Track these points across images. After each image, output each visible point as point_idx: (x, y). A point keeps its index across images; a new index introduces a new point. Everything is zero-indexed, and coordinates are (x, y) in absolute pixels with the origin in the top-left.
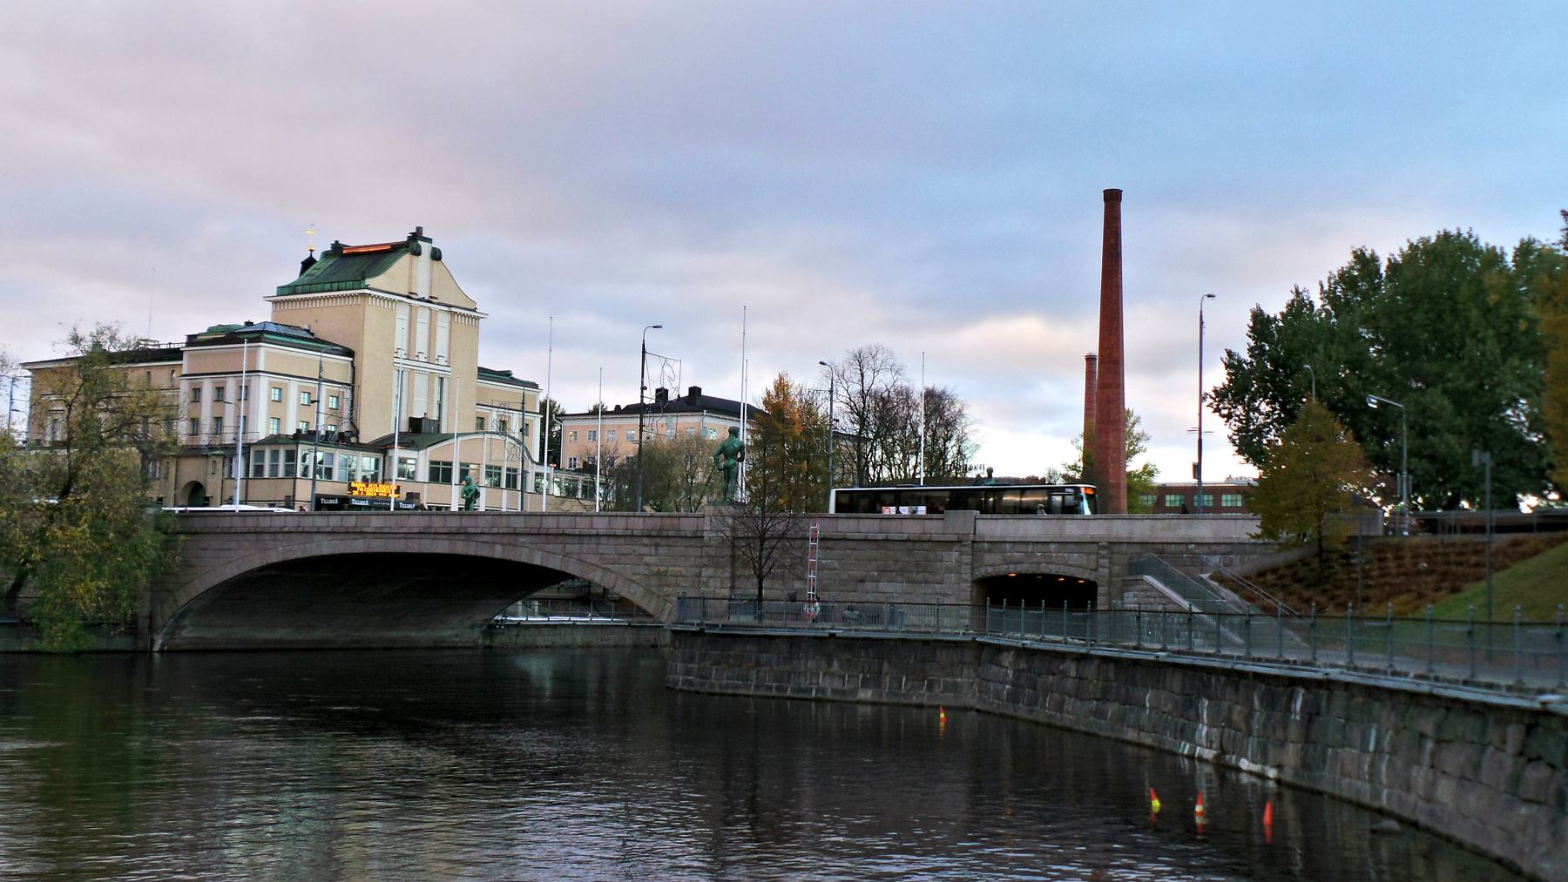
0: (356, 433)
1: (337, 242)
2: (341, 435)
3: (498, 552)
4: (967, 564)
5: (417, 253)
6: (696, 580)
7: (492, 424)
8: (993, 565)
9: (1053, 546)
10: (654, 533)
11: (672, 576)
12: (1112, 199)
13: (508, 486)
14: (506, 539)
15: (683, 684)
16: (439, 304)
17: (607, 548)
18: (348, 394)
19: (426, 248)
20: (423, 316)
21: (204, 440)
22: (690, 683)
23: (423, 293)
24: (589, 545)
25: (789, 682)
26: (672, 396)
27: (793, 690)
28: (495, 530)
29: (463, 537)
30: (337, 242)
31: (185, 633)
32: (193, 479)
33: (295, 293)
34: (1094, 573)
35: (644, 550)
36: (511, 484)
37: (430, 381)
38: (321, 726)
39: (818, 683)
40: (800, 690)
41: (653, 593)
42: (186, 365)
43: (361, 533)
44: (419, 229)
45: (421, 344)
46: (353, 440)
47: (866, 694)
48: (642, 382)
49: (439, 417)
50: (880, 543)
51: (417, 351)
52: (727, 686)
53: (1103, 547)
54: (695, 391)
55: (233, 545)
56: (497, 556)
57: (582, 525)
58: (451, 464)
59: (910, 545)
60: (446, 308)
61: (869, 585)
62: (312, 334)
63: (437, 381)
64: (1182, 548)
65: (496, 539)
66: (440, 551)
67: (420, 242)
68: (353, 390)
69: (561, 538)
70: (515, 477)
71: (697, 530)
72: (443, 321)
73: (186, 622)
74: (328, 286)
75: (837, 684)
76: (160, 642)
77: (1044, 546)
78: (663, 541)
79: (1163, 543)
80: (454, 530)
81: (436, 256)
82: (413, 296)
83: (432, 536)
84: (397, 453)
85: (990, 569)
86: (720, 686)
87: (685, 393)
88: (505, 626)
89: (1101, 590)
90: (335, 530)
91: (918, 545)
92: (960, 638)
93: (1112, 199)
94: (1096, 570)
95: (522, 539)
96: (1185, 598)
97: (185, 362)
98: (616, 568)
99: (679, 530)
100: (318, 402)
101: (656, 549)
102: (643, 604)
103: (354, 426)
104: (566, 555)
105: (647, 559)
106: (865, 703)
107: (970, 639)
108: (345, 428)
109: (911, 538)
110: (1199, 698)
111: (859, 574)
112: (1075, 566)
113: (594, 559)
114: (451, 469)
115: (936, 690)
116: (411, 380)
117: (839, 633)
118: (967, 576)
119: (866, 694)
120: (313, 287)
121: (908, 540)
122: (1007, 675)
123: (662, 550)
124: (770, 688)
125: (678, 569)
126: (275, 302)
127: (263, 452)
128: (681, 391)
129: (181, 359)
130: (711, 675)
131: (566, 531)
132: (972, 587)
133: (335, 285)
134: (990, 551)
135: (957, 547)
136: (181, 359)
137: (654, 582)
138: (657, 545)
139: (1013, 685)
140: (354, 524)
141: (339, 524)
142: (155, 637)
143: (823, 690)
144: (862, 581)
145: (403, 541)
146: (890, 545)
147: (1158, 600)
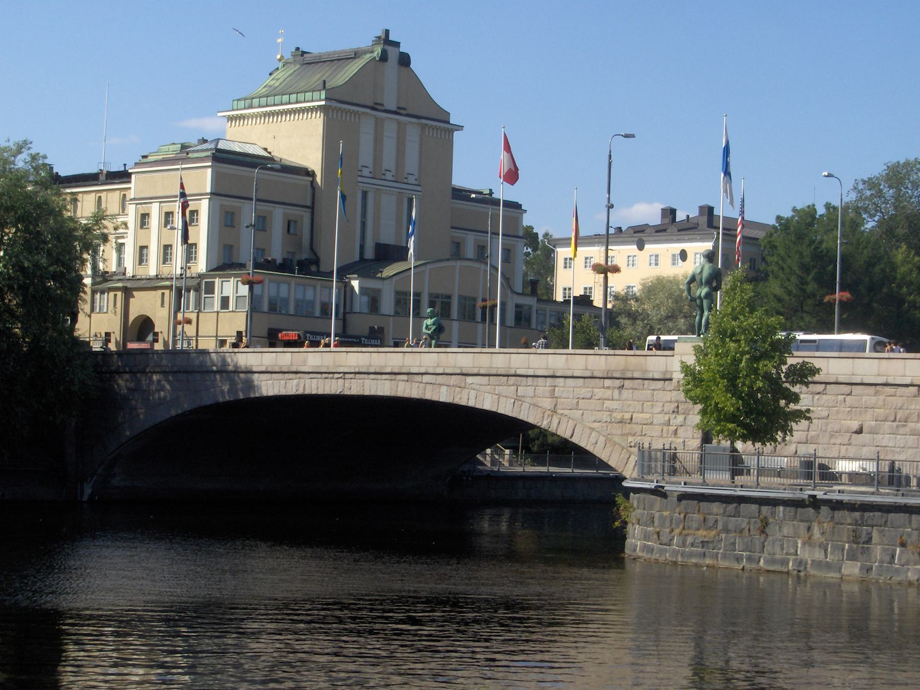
0: (317, 262)
3: (443, 395)
6: (665, 428)
10: (616, 375)
11: (637, 423)
15: (642, 550)
16: (408, 115)
18: (306, 216)
19: (392, 52)
21: (152, 269)
22: (651, 550)
23: (391, 105)
25: (762, 551)
26: (680, 216)
27: (766, 562)
29: (405, 377)
32: (148, 315)
35: (608, 393)
38: (219, 605)
39: (796, 554)
40: (773, 561)
41: (615, 444)
42: (134, 187)
44: (387, 32)
46: (313, 268)
51: (361, 164)
52: (691, 555)
56: (443, 399)
60: (415, 120)
61: (864, 437)
62: (270, 153)
65: (440, 379)
66: (380, 393)
68: (313, 213)
69: (512, 380)
71: (667, 371)
72: (413, 134)
74: (285, 98)
75: (818, 555)
78: (627, 382)
80: (396, 371)
81: (405, 60)
82: (379, 107)
87: (694, 213)
90: (270, 369)
95: (470, 380)
96: (898, 560)
97: (132, 185)
99: (646, 371)
101: (620, 393)
102: (603, 456)
103: (315, 254)
105: (607, 404)
108: (305, 255)
114: (449, 303)
117: (820, 494)
119: (852, 569)
123: (626, 394)
124: (738, 559)
129: (130, 182)
131: (519, 372)
133: (293, 97)
136: (130, 182)
137: (617, 430)
140: (288, 363)
141: (258, 363)
144: (860, 431)
145: (341, 381)
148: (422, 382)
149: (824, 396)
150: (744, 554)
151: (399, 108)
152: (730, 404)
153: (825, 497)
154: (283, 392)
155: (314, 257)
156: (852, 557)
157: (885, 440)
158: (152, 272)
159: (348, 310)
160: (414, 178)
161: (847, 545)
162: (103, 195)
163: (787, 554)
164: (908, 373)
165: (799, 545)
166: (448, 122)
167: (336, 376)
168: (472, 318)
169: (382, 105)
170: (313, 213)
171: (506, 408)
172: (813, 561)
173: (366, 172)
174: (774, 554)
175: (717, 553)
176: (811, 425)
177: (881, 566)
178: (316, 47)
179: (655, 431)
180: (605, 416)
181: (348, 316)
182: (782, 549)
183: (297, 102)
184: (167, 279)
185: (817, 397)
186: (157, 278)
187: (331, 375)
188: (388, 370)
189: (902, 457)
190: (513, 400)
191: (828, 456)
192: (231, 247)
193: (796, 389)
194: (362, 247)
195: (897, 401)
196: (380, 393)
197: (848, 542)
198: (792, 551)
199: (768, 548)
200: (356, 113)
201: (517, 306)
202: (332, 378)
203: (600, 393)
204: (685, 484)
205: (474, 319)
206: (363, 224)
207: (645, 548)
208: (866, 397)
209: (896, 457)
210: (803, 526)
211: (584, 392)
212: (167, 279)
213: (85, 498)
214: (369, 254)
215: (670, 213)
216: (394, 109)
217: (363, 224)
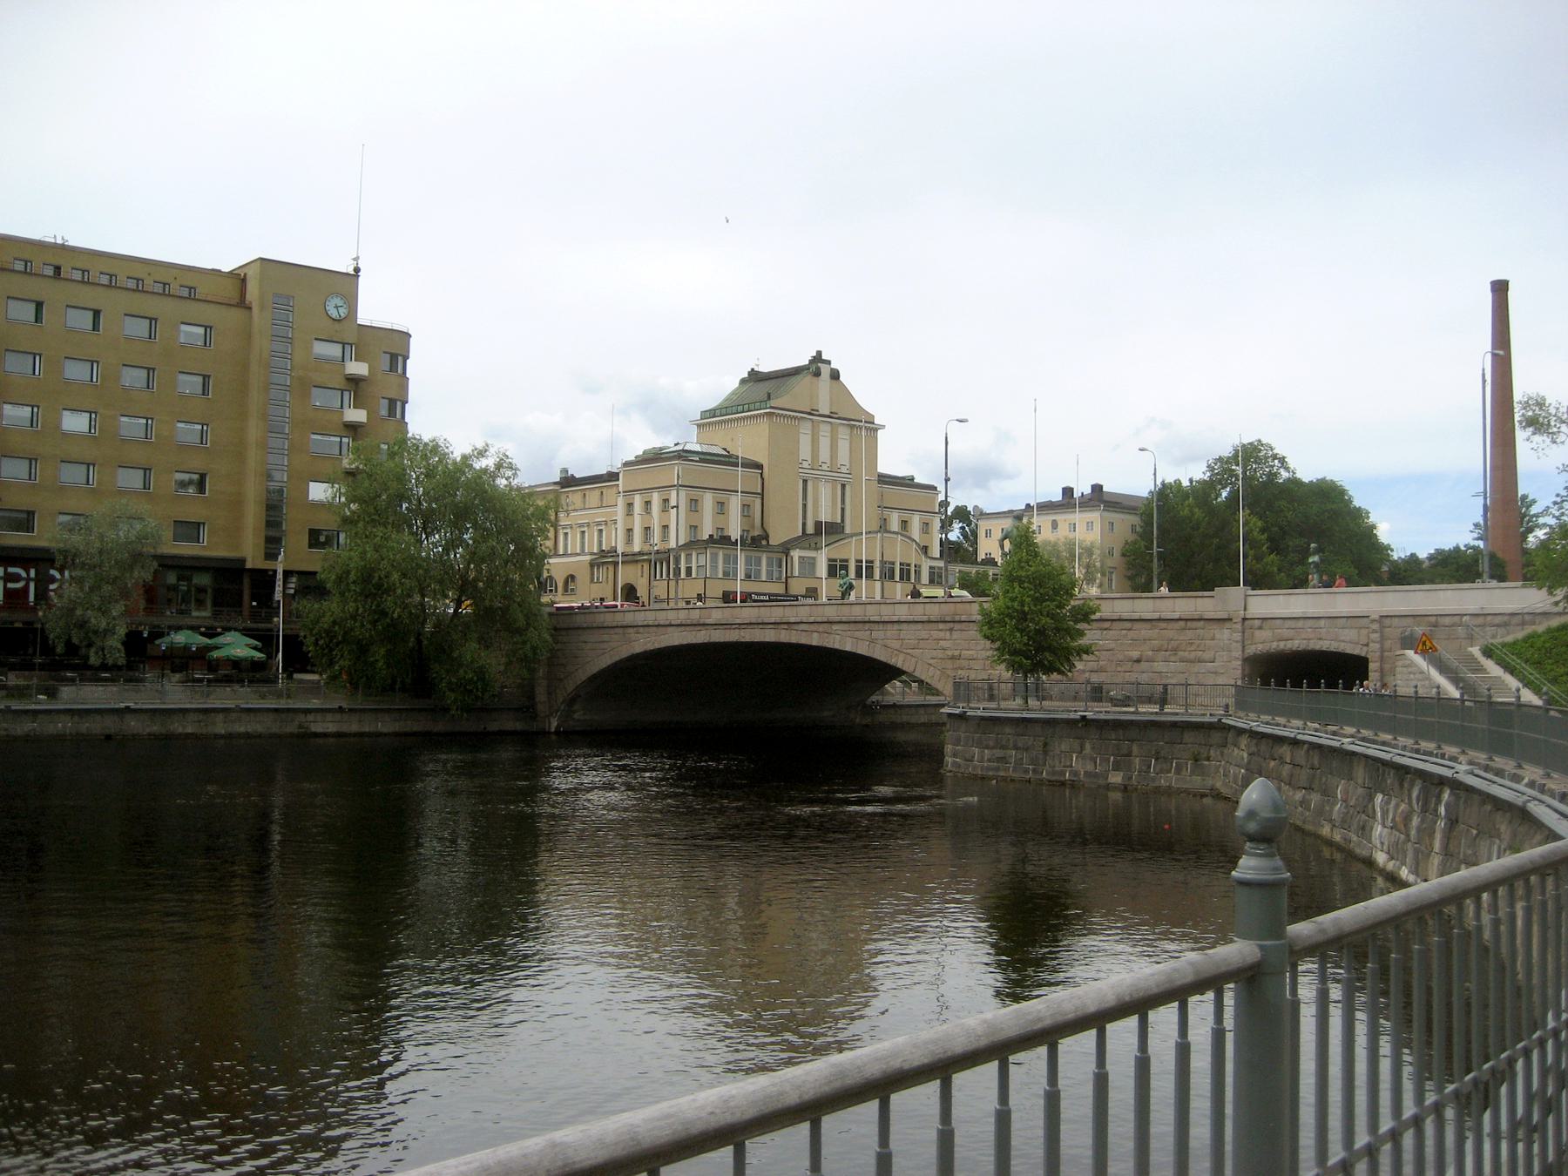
0: (766, 537)
1: (753, 370)
2: (753, 539)
3: (815, 640)
4: (1237, 642)
5: (817, 374)
7: (895, 525)
8: (1266, 642)
9: (1322, 622)
10: (948, 619)
12: (1500, 289)
13: (901, 578)
14: (821, 628)
16: (839, 418)
17: (909, 633)
18: (758, 502)
19: (825, 370)
20: (825, 430)
24: (891, 631)
28: (812, 619)
29: (786, 627)
30: (753, 370)
31: (576, 716)
33: (714, 416)
34: (1365, 649)
35: (941, 634)
36: (905, 575)
37: (834, 489)
39: (1071, 766)
40: (1054, 773)
43: (704, 625)
44: (819, 353)
45: (824, 455)
46: (764, 542)
47: (1116, 778)
48: (946, 473)
49: (843, 520)
50: (1154, 623)
52: (988, 769)
53: (1373, 621)
54: (1097, 489)
55: (606, 638)
57: (886, 613)
58: (847, 561)
59: (1182, 623)
61: (1144, 665)
62: (728, 452)
63: (839, 487)
64: (1456, 619)
65: (812, 627)
67: (819, 364)
68: (763, 499)
69: (867, 626)
70: (909, 571)
73: (576, 707)
75: (1090, 767)
76: (556, 724)
77: (1315, 621)
78: (957, 626)
79: (1437, 615)
80: (694, 622)
81: (835, 375)
82: (815, 412)
83: (761, 626)
84: (796, 554)
85: (1260, 647)
86: (982, 769)
87: (1088, 491)
88: (881, 707)
89: (1372, 666)
91: (1189, 623)
92: (1207, 719)
93: (1500, 289)
94: (1367, 645)
95: (835, 627)
97: (620, 482)
98: (917, 652)
100: (677, 507)
104: (873, 641)
106: (1115, 788)
107: (1216, 720)
108: (757, 532)
109: (1183, 617)
110: (1376, 792)
111: (1135, 654)
112: (1346, 642)
113: (895, 644)
115: (1184, 773)
116: (816, 489)
117: (1089, 715)
118: (1238, 654)
119: (1116, 778)
120: (729, 410)
121: (1180, 619)
122: (1243, 758)
123: (956, 635)
124: (1027, 771)
125: (970, 652)
126: (699, 426)
127: (691, 555)
128: (1082, 488)
130: (973, 757)
132: (1243, 665)
134: (1260, 628)
135: (1228, 625)
136: (618, 480)
137: (949, 664)
138: (951, 630)
139: (1247, 770)
142: (552, 719)
143: (1076, 774)
144: (1138, 661)
146: (1163, 625)
147: (1417, 676)
148: (1357, 643)
149: (1111, 632)
150: (1031, 767)
151: (831, 413)
152: (1018, 640)
153: (1094, 717)
154: (694, 641)
155: (765, 534)
156: (1117, 767)
157: (1159, 666)
158: (637, 549)
159: (789, 575)
160: (807, 463)
161: (1112, 758)
162: (604, 491)
163: (1064, 767)
164: (1177, 609)
165: (1074, 759)
166: (873, 423)
167: (734, 626)
168: (892, 577)
169: (817, 411)
170: (763, 499)
171: (863, 650)
172: (1085, 772)
173: (805, 465)
174: (1054, 767)
175: (1009, 767)
176: (1144, 658)
177: (1140, 775)
178: (765, 368)
179: (977, 665)
180: (940, 654)
181: (789, 580)
182: (1060, 762)
183: (749, 411)
184: (647, 554)
185: (1105, 632)
186: (640, 553)
187: (729, 626)
188: (773, 620)
189: (1174, 681)
190: (868, 643)
191: (1115, 681)
192: (696, 527)
193: (1080, 626)
194: (804, 524)
195: (1170, 634)
196: (767, 640)
197: (1113, 755)
198: (1068, 764)
199: (1049, 762)
200: (795, 418)
201: (930, 568)
202: (730, 629)
203: (936, 634)
204: (1211, 715)
205: (893, 579)
206: (805, 506)
207: (954, 763)
208: (1144, 631)
209: (1168, 682)
210: (1076, 744)
211: (924, 634)
212: (647, 554)
213: (553, 730)
214: (810, 529)
215: (1068, 492)
216: (827, 412)
217: (805, 506)
